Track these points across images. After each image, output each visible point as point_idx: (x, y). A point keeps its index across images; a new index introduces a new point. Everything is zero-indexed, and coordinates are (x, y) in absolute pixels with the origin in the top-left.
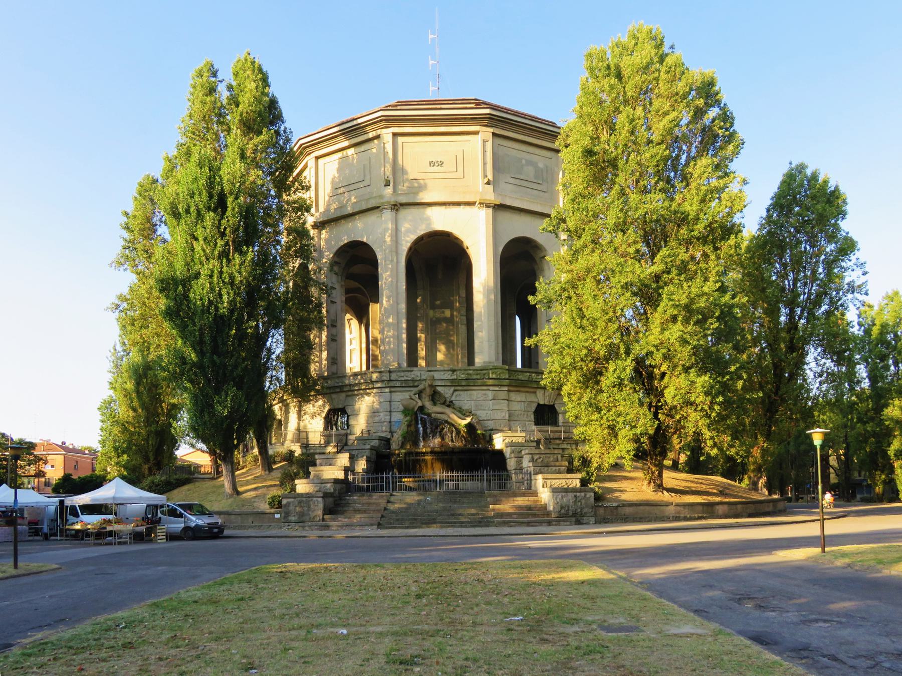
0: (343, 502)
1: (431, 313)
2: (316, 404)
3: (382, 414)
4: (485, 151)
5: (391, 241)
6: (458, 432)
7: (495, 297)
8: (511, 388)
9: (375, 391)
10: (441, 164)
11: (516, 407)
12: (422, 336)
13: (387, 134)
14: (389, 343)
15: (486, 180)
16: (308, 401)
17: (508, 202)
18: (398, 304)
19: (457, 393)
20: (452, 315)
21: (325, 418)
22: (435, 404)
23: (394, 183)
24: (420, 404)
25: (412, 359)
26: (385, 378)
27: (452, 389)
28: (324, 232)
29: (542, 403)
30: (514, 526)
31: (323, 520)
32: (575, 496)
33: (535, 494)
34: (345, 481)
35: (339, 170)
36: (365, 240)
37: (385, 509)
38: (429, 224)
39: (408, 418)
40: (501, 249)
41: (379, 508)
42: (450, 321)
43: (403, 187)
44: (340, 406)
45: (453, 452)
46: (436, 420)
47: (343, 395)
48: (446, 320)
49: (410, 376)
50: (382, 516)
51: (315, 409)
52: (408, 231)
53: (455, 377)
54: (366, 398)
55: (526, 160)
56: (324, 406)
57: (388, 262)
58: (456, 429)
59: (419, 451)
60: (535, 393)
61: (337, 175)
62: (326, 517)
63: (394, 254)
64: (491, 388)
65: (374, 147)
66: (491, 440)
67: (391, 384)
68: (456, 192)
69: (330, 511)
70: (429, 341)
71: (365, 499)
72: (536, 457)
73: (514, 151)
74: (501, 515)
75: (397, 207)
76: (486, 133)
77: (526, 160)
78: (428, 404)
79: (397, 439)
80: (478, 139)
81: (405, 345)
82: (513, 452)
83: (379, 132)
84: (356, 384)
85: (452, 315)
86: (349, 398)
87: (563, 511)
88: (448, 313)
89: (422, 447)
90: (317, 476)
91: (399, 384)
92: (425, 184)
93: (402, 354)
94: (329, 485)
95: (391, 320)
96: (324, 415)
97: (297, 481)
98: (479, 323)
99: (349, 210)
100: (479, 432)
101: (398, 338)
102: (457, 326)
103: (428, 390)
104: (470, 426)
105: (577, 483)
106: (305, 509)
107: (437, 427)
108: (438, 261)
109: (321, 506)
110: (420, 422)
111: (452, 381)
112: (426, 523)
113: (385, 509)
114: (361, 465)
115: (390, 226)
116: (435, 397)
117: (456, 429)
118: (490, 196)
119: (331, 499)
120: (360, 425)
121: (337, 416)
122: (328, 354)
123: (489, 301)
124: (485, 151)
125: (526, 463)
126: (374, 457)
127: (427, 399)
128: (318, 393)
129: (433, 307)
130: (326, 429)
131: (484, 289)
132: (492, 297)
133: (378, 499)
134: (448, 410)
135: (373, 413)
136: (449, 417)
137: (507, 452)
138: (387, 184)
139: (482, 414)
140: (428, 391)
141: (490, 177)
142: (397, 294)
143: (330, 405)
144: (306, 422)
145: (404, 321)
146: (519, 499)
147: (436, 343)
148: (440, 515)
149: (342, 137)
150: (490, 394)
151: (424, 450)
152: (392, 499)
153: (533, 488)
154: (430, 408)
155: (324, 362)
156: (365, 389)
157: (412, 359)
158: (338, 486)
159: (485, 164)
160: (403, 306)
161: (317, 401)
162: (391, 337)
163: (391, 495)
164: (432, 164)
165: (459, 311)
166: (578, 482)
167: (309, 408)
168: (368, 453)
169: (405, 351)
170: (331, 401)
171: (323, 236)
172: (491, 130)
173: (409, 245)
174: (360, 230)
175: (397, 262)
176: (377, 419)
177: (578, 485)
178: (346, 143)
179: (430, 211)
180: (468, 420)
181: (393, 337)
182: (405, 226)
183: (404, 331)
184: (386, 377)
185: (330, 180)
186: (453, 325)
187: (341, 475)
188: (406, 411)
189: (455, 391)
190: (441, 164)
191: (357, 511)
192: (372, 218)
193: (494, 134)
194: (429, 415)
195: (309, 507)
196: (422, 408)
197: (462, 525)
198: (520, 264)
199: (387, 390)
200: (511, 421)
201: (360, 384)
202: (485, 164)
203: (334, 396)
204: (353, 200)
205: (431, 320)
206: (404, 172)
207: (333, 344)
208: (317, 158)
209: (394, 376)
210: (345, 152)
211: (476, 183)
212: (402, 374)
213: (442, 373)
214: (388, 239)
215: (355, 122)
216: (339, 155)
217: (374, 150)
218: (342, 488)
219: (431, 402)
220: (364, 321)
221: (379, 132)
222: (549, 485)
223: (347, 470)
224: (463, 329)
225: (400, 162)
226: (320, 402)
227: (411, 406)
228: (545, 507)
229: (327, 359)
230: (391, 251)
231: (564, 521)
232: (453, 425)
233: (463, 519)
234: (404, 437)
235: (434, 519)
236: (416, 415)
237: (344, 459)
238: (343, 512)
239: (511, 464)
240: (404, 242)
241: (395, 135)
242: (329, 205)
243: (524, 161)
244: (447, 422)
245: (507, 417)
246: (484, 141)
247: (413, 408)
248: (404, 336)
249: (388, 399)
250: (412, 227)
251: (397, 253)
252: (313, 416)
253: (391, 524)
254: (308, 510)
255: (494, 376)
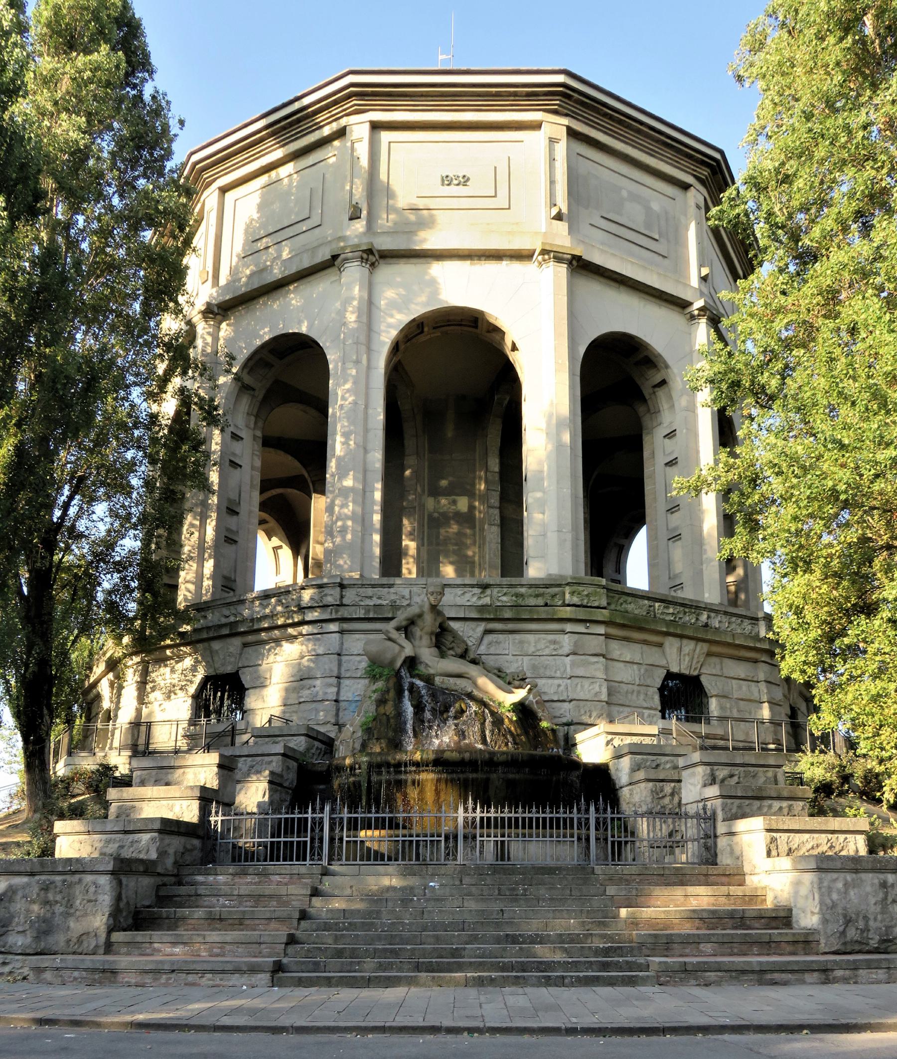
0: (183, 890)
1: (430, 503)
2: (179, 667)
3: (318, 682)
4: (552, 160)
5: (356, 332)
6: (498, 721)
7: (570, 438)
8: (613, 631)
9: (305, 629)
10: (465, 181)
11: (624, 674)
12: (410, 545)
13: (359, 126)
14: (343, 530)
15: (554, 211)
16: (162, 661)
17: (597, 259)
18: (366, 451)
19: (489, 638)
20: (472, 508)
21: (196, 697)
22: (443, 655)
23: (369, 213)
24: (408, 651)
25: (391, 561)
26: (329, 600)
27: (481, 627)
28: (224, 325)
29: (675, 669)
30: (718, 983)
31: (109, 947)
32: (884, 885)
33: (737, 876)
34: (198, 831)
35: (261, 207)
36: (304, 330)
37: (304, 915)
38: (435, 292)
39: (380, 684)
40: (582, 350)
41: (282, 912)
42: (468, 519)
43: (385, 221)
44: (229, 669)
45: (490, 762)
46: (443, 691)
47: (237, 642)
48: (459, 517)
49: (387, 597)
50: (292, 940)
51: (176, 678)
52: (393, 304)
53: (487, 600)
54: (286, 645)
55: (630, 193)
56: (194, 669)
57: (349, 365)
58: (493, 713)
59: (405, 757)
60: (660, 645)
61: (256, 216)
62: (117, 936)
63: (363, 348)
64: (569, 627)
65: (331, 154)
66: (570, 745)
67: (344, 613)
68: (496, 238)
69: (135, 918)
70: (425, 556)
71: (247, 884)
72: (722, 773)
73: (605, 171)
74: (663, 942)
75: (374, 257)
76: (556, 126)
77: (630, 193)
78: (427, 655)
79: (354, 724)
80: (535, 141)
81: (377, 538)
82: (636, 768)
83: (343, 122)
84: (265, 617)
85: (472, 508)
86: (249, 650)
87: (852, 933)
88: (463, 504)
89: (412, 750)
90: (125, 813)
91: (361, 614)
92: (432, 216)
93: (372, 556)
94: (146, 837)
95: (348, 482)
96: (192, 689)
97: (59, 826)
98: (539, 495)
99: (277, 273)
100: (544, 724)
101: (363, 520)
102: (482, 530)
103: (428, 618)
104: (521, 708)
105: (858, 846)
106: (59, 909)
107: (443, 704)
108: (454, 383)
109: (106, 900)
110: (408, 693)
111: (482, 608)
112: (430, 968)
113: (304, 915)
114: (254, 794)
115: (356, 290)
116: (442, 638)
117: (493, 713)
118: (562, 238)
119: (146, 882)
120: (266, 704)
121: (223, 691)
122: (216, 566)
123: (559, 446)
124: (552, 160)
125: (695, 789)
126: (291, 778)
127: (426, 641)
128: (186, 640)
129: (435, 492)
130: (193, 722)
131: (549, 423)
132: (566, 438)
133: (287, 882)
134: (472, 670)
135: (301, 679)
136: (475, 684)
137: (622, 771)
138: (355, 216)
139: (550, 688)
140: (429, 622)
141: (563, 204)
142: (366, 430)
143: (208, 666)
144: (155, 707)
145: (379, 485)
146: (701, 890)
147: (438, 562)
148: (474, 939)
149: (270, 142)
150: (566, 642)
151: (418, 756)
152: (327, 884)
153: (724, 859)
154: (432, 662)
155: (207, 583)
156: (285, 626)
157: (391, 561)
158: (176, 843)
159: (552, 182)
160: (377, 457)
161: (180, 658)
162: (347, 517)
163: (325, 873)
164: (447, 181)
165: (484, 498)
166: (861, 840)
167: (163, 675)
168: (276, 764)
169: (377, 551)
170: (209, 658)
171: (222, 334)
172: (565, 121)
173: (394, 333)
174: (294, 313)
175: (369, 368)
176: (306, 694)
177: (863, 851)
178: (279, 154)
179: (437, 269)
180: (520, 694)
181: (353, 517)
182: (387, 295)
183: (378, 508)
184: (332, 597)
185: (243, 227)
186: (473, 527)
187: (189, 812)
188: (376, 668)
189: (487, 632)
190: (465, 181)
191: (216, 921)
192: (320, 287)
193: (572, 133)
194: (428, 680)
195: (70, 904)
196: (412, 663)
197: (548, 975)
198: (617, 383)
199: (333, 627)
200: (613, 705)
201: (273, 615)
202: (552, 182)
203: (216, 645)
204: (285, 255)
205: (430, 516)
206: (389, 193)
207: (229, 549)
208: (224, 190)
209: (350, 596)
210: (273, 173)
211: (535, 220)
212: (370, 591)
213: (459, 591)
214: (351, 317)
215: (297, 106)
216: (263, 179)
217: (332, 160)
218: (186, 850)
219: (434, 650)
220: (303, 551)
221: (343, 122)
222: (783, 848)
223: (206, 797)
224: (493, 534)
225: (383, 176)
226: (188, 662)
227: (389, 656)
228: (782, 918)
229: (213, 577)
230: (357, 343)
231: (869, 965)
232: (485, 705)
233: (544, 953)
234: (368, 731)
235: (456, 953)
236: (398, 680)
237: (203, 769)
238: (173, 924)
239: (635, 796)
240: (383, 327)
241: (376, 126)
242: (234, 272)
243: (624, 194)
244: (470, 696)
245: (604, 697)
246: (552, 141)
247: (392, 662)
248: (377, 518)
249: (336, 649)
250: (401, 300)
251: (369, 350)
252: (169, 694)
253: (316, 967)
254: (67, 915)
255: (576, 600)
